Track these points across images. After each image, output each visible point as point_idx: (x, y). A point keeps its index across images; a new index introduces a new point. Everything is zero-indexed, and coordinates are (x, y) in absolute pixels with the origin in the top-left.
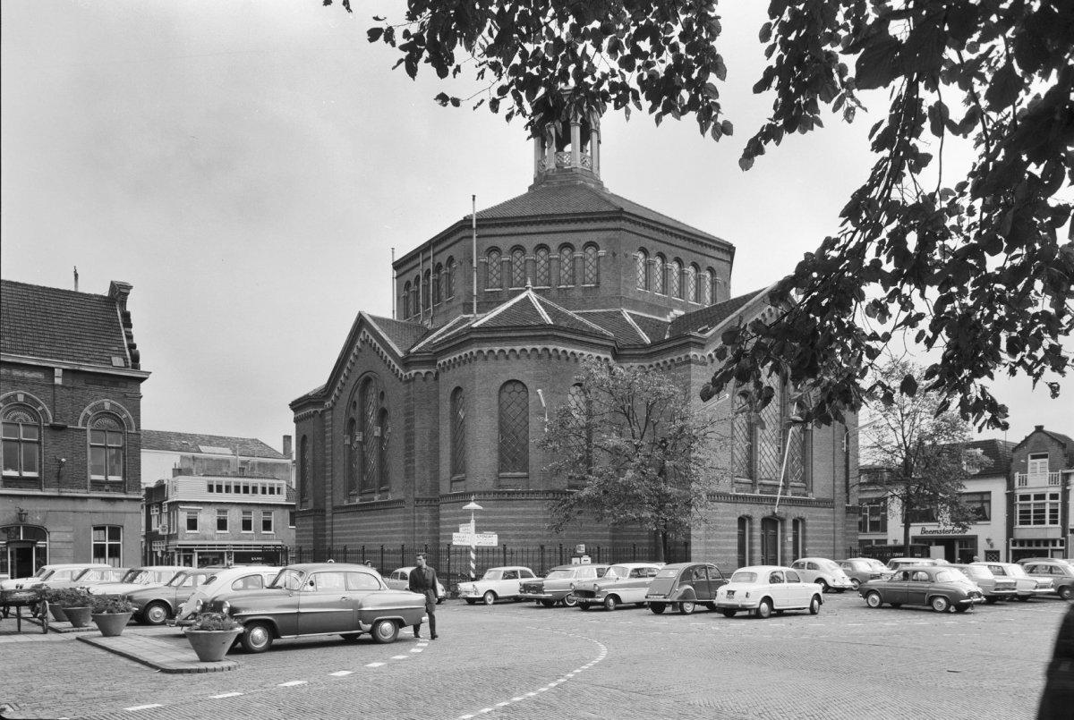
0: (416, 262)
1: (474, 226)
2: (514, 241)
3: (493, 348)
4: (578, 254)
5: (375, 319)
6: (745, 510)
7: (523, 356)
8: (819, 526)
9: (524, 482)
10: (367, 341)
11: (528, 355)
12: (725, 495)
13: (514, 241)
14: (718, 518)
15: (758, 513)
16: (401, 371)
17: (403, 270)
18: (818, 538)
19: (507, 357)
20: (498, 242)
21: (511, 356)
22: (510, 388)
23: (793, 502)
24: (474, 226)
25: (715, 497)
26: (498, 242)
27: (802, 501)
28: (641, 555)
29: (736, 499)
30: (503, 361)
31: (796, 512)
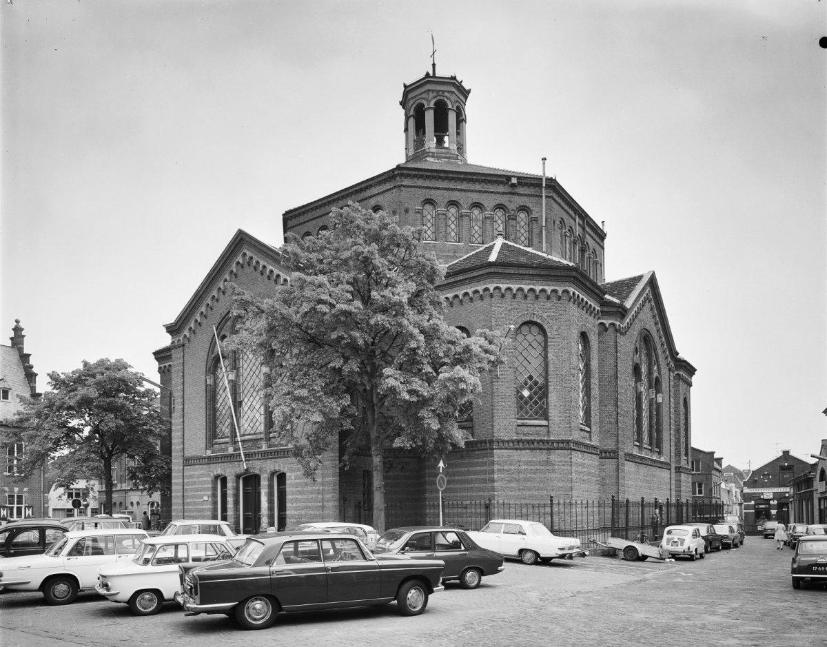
1: (544, 185)
2: (475, 197)
3: (488, 286)
4: (441, 210)
6: (218, 469)
7: (543, 297)
8: (478, 463)
9: (545, 430)
11: (461, 301)
12: (201, 458)
13: (475, 197)
14: (194, 480)
15: (230, 471)
18: (300, 493)
19: (559, 298)
20: (433, 194)
21: (565, 297)
22: (535, 329)
23: (266, 455)
24: (544, 185)
25: (188, 461)
26: (433, 194)
27: (222, 457)
28: (542, 510)
29: (210, 460)
30: (487, 300)
31: (271, 465)
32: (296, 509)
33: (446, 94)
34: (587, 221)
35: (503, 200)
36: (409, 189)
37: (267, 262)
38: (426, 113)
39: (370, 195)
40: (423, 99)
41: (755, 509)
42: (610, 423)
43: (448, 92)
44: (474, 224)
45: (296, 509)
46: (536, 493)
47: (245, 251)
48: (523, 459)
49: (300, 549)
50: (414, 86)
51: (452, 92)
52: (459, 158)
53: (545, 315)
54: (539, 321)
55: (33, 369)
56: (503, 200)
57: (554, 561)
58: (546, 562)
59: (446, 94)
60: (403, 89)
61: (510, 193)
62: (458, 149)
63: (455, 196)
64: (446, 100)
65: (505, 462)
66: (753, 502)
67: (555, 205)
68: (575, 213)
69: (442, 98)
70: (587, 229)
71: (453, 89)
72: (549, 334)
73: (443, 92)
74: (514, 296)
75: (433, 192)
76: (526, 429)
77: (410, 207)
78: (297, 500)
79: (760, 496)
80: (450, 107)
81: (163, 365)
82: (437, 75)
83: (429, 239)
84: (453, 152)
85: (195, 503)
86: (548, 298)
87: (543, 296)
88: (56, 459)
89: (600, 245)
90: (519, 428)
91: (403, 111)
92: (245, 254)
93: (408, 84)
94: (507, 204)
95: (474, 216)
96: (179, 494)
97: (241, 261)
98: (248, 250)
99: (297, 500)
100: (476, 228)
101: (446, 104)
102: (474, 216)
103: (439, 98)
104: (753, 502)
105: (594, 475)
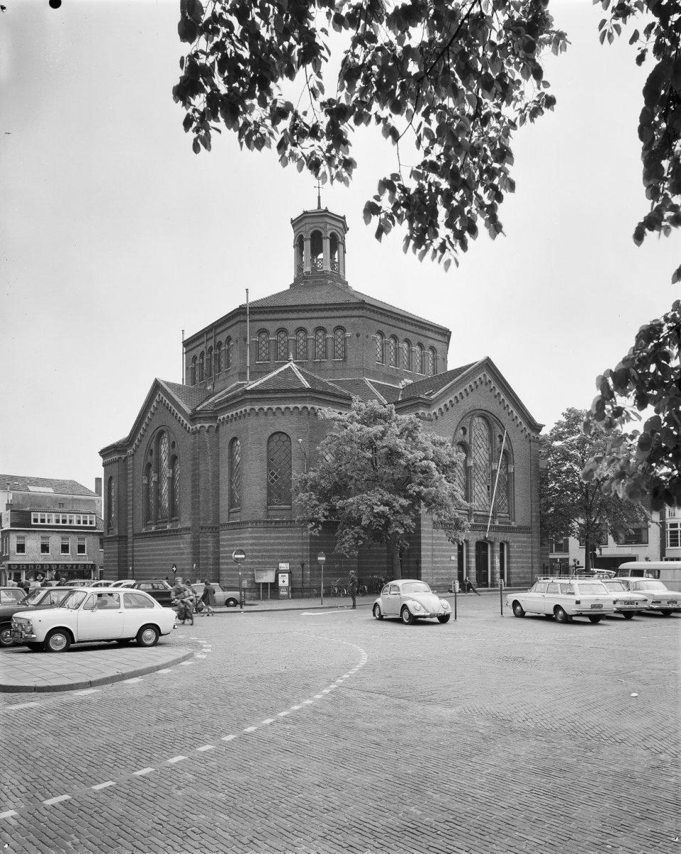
0: (201, 341)
5: (168, 384)
7: (287, 413)
10: (162, 401)
16: (189, 425)
17: (190, 347)
32: (517, 568)
37: (442, 402)
38: (324, 241)
39: (429, 336)
42: (64, 521)
45: (517, 568)
49: (26, 595)
57: (574, 618)
58: (415, 621)
63: (322, 323)
74: (309, 413)
78: (518, 562)
85: (442, 562)
86: (300, 413)
87: (287, 412)
88: (654, 533)
96: (429, 553)
99: (518, 562)
105: (223, 564)
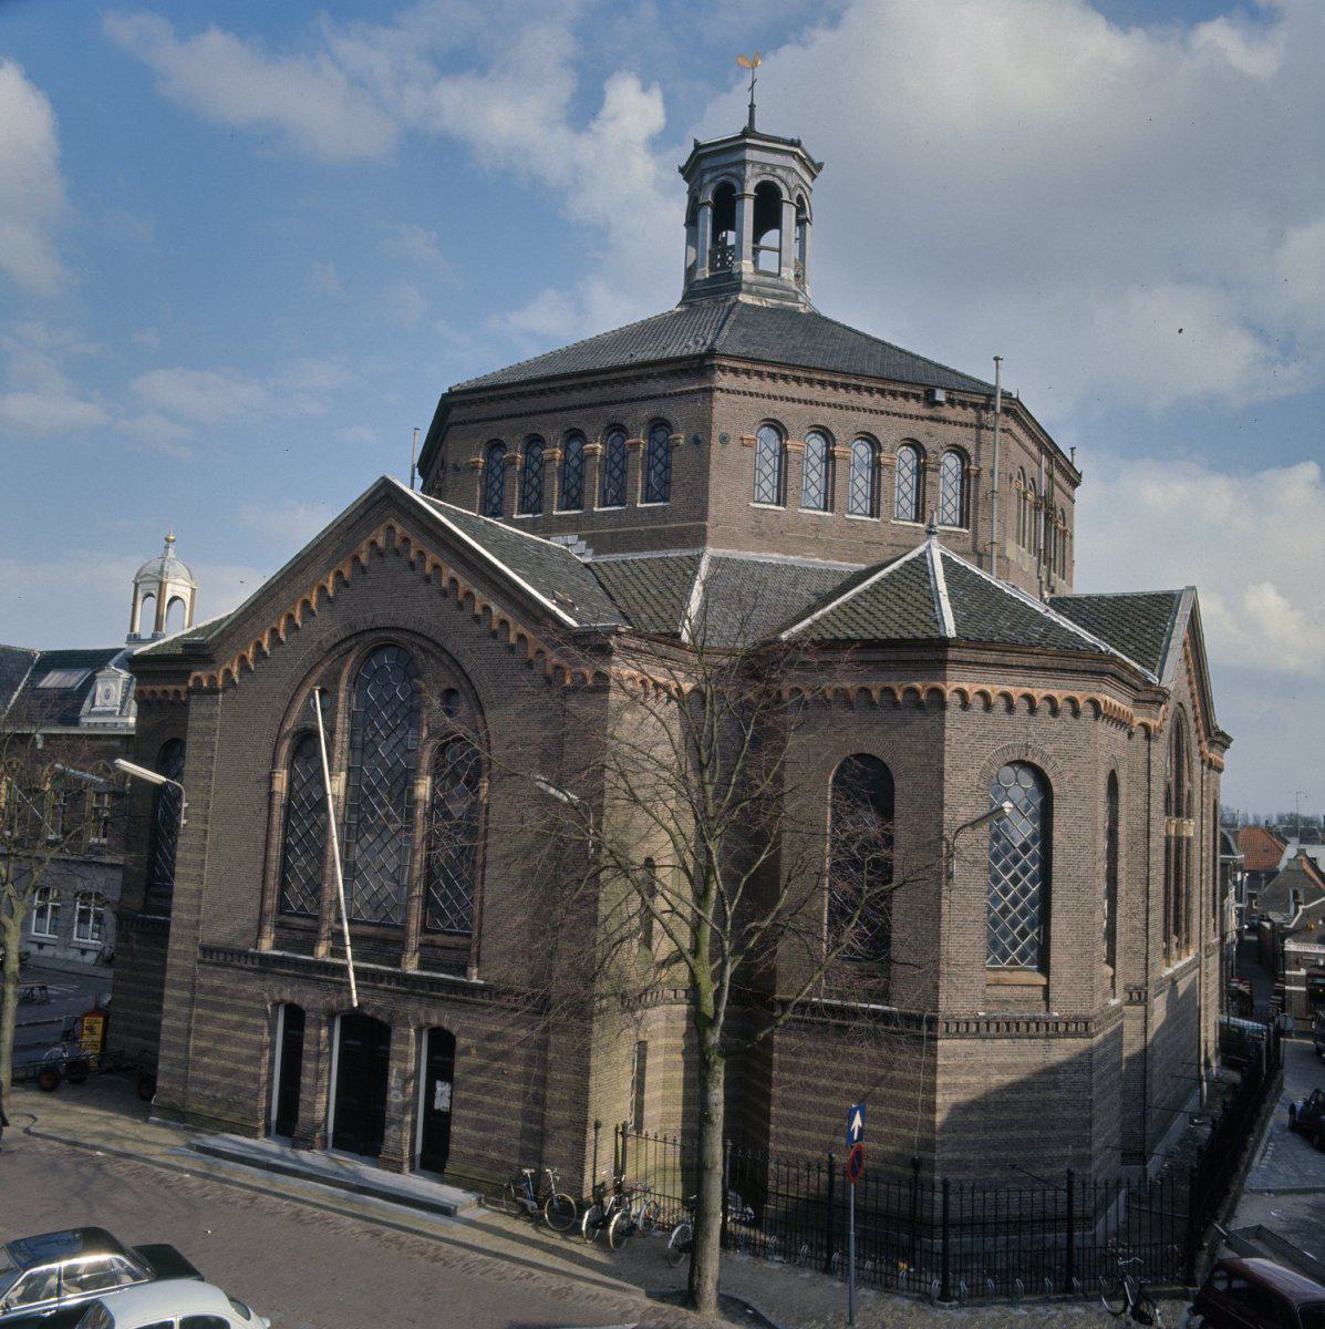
2: (863, 421)
13: (863, 421)
33: (779, 172)
34: (1057, 460)
35: (918, 430)
36: (732, 397)
40: (732, 175)
41: (1307, 985)
43: (784, 168)
44: (856, 473)
46: (1017, 1134)
47: (391, 521)
48: (996, 1060)
50: (714, 148)
51: (792, 170)
52: (801, 299)
53: (1049, 749)
54: (1036, 761)
55: (4, 1128)
56: (918, 430)
59: (779, 172)
60: (692, 148)
61: (931, 419)
62: (797, 276)
64: (778, 182)
65: (960, 1067)
66: (1303, 972)
67: (1013, 445)
68: (1040, 450)
69: (770, 178)
70: (1057, 476)
71: (795, 164)
72: (1055, 789)
73: (774, 167)
75: (779, 404)
76: (1003, 992)
77: (731, 433)
79: (1317, 960)
80: (785, 196)
81: (149, 688)
82: (758, 128)
83: (765, 499)
84: (786, 284)
89: (1069, 496)
90: (988, 990)
91: (687, 186)
92: (391, 528)
93: (703, 141)
94: (922, 439)
95: (857, 458)
97: (381, 542)
98: (399, 521)
100: (860, 482)
101: (778, 193)
102: (857, 458)
103: (765, 178)
104: (1303, 972)
